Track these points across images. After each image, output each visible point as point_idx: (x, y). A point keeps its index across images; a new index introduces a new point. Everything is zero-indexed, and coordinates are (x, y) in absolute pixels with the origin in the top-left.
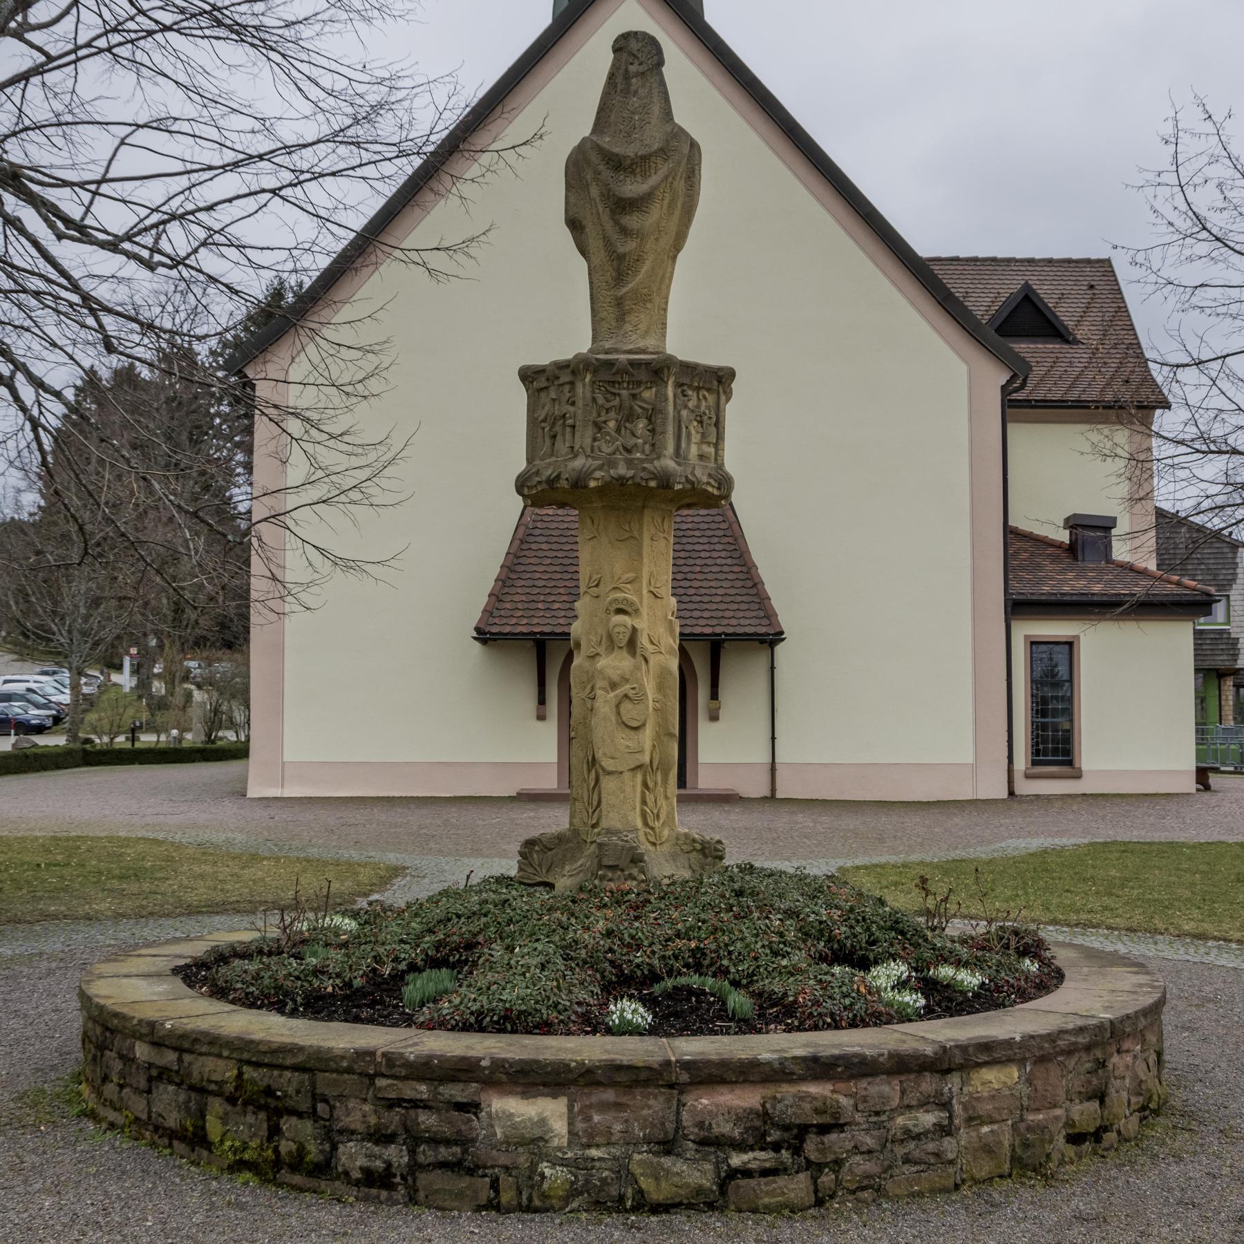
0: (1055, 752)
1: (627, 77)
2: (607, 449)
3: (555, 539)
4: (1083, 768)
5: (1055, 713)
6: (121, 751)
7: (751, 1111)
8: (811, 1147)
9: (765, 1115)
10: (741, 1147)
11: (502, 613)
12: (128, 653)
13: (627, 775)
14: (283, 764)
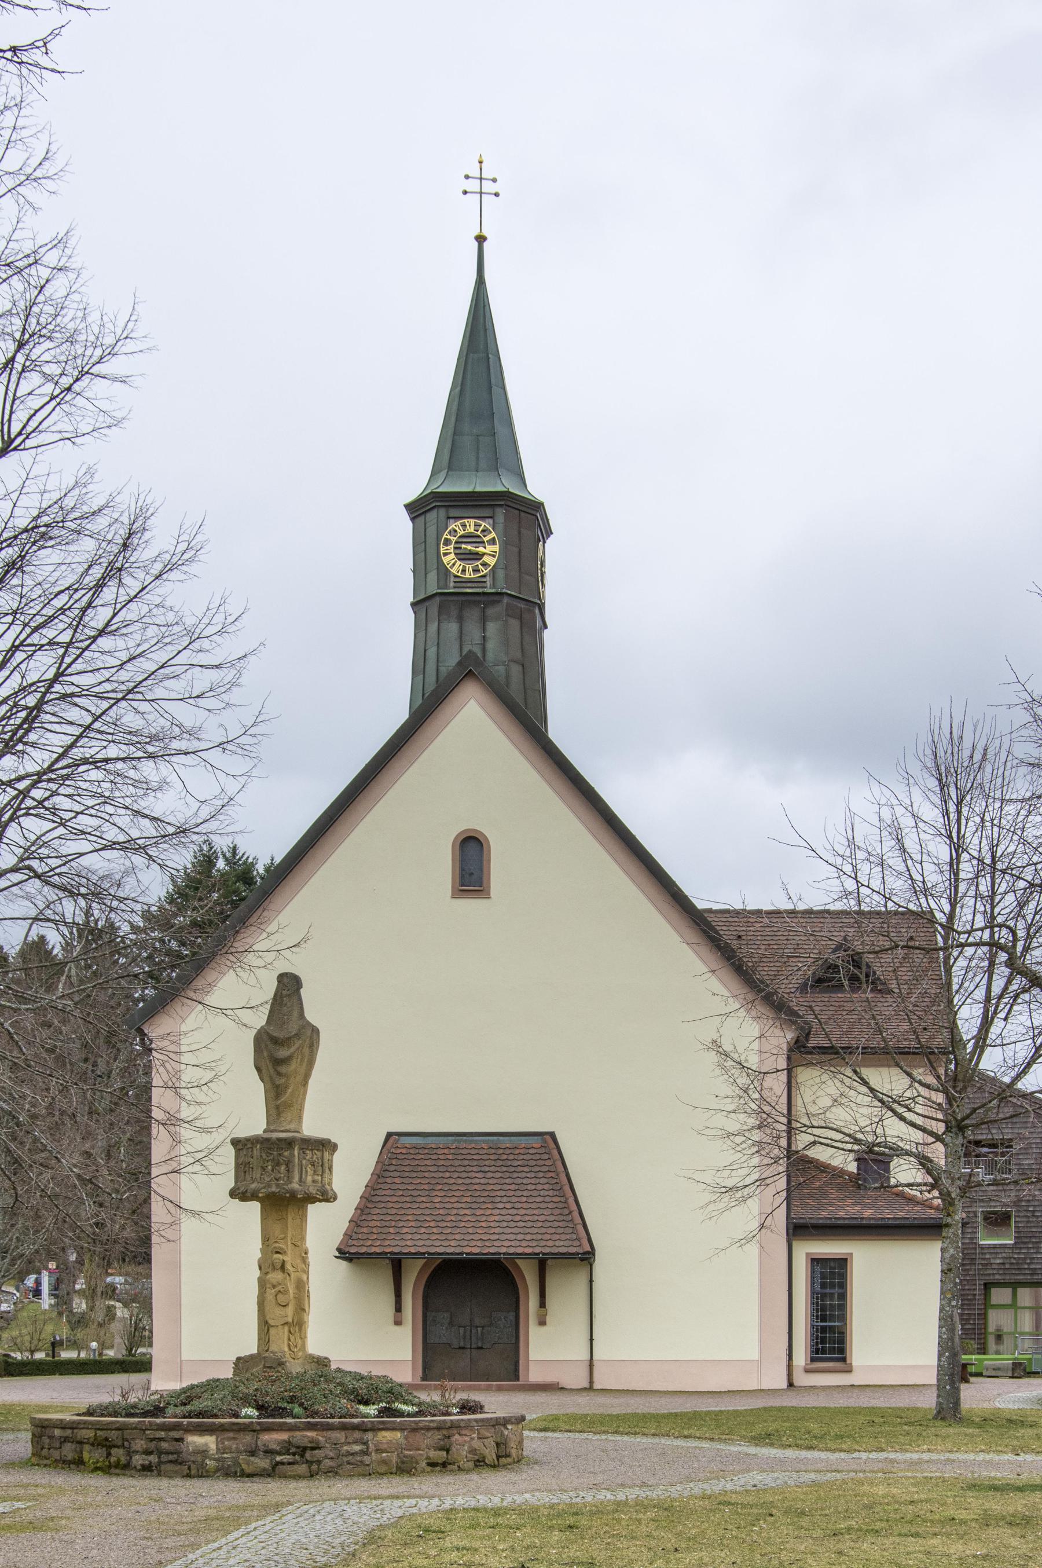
0: (832, 1350)
1: (282, 997)
2: (267, 1179)
3: (407, 1174)
4: (854, 1364)
5: (832, 1318)
6: (41, 1362)
7: (284, 1440)
8: (308, 1455)
9: (289, 1442)
10: (280, 1454)
11: (360, 1236)
12: (46, 1268)
13: (280, 1327)
14: (181, 1362)
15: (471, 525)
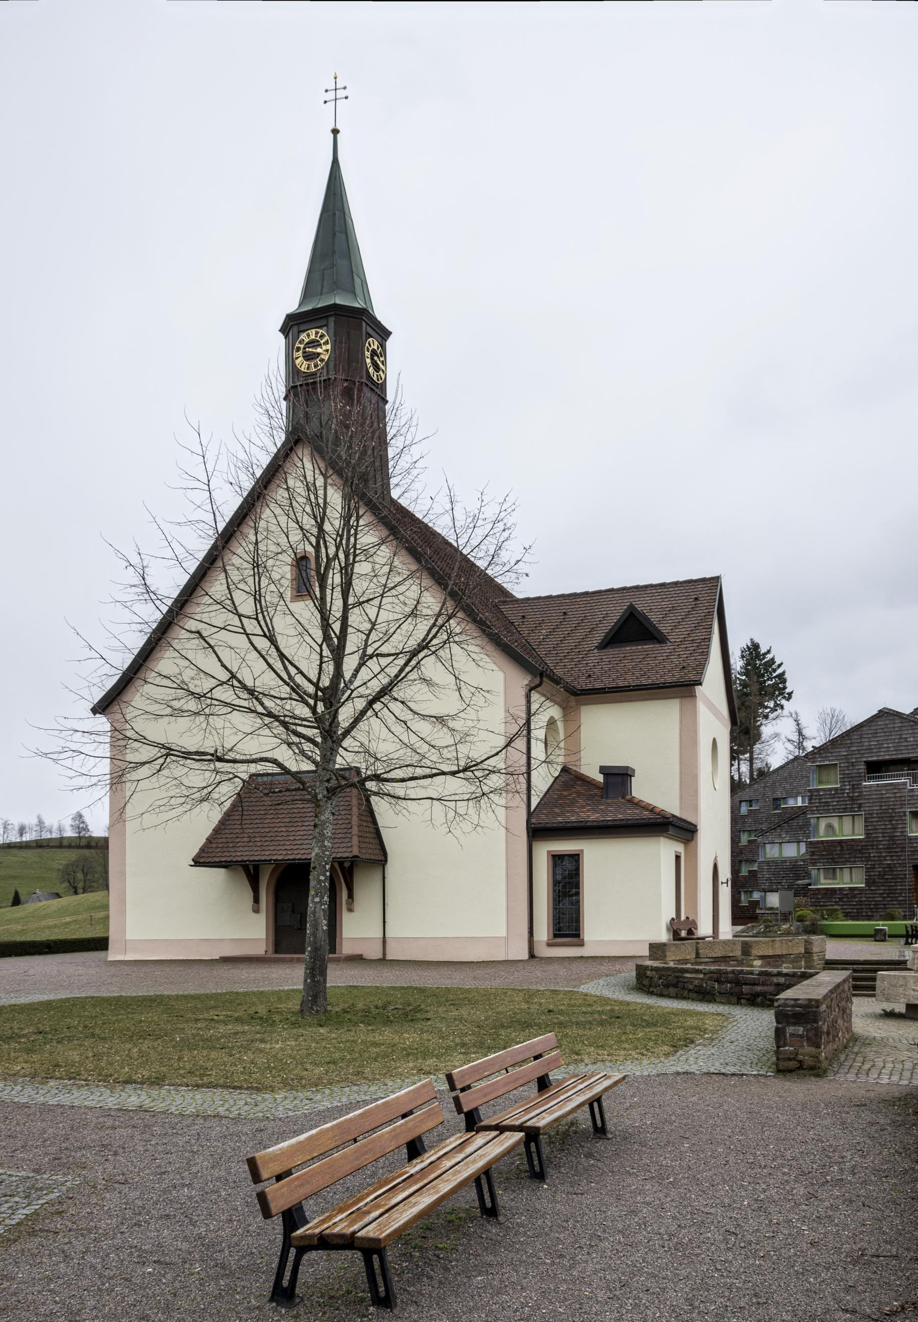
15: (312, 334)
